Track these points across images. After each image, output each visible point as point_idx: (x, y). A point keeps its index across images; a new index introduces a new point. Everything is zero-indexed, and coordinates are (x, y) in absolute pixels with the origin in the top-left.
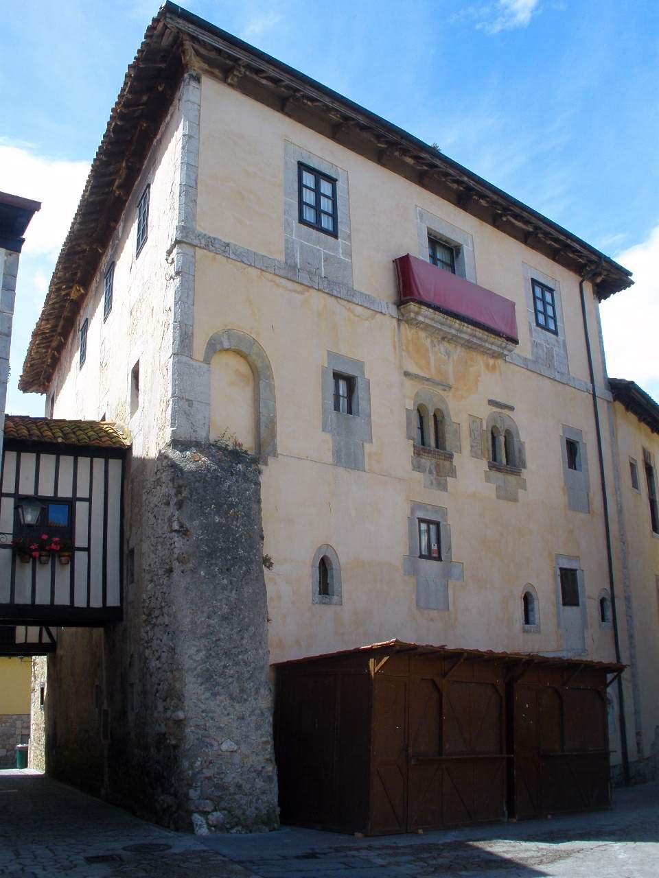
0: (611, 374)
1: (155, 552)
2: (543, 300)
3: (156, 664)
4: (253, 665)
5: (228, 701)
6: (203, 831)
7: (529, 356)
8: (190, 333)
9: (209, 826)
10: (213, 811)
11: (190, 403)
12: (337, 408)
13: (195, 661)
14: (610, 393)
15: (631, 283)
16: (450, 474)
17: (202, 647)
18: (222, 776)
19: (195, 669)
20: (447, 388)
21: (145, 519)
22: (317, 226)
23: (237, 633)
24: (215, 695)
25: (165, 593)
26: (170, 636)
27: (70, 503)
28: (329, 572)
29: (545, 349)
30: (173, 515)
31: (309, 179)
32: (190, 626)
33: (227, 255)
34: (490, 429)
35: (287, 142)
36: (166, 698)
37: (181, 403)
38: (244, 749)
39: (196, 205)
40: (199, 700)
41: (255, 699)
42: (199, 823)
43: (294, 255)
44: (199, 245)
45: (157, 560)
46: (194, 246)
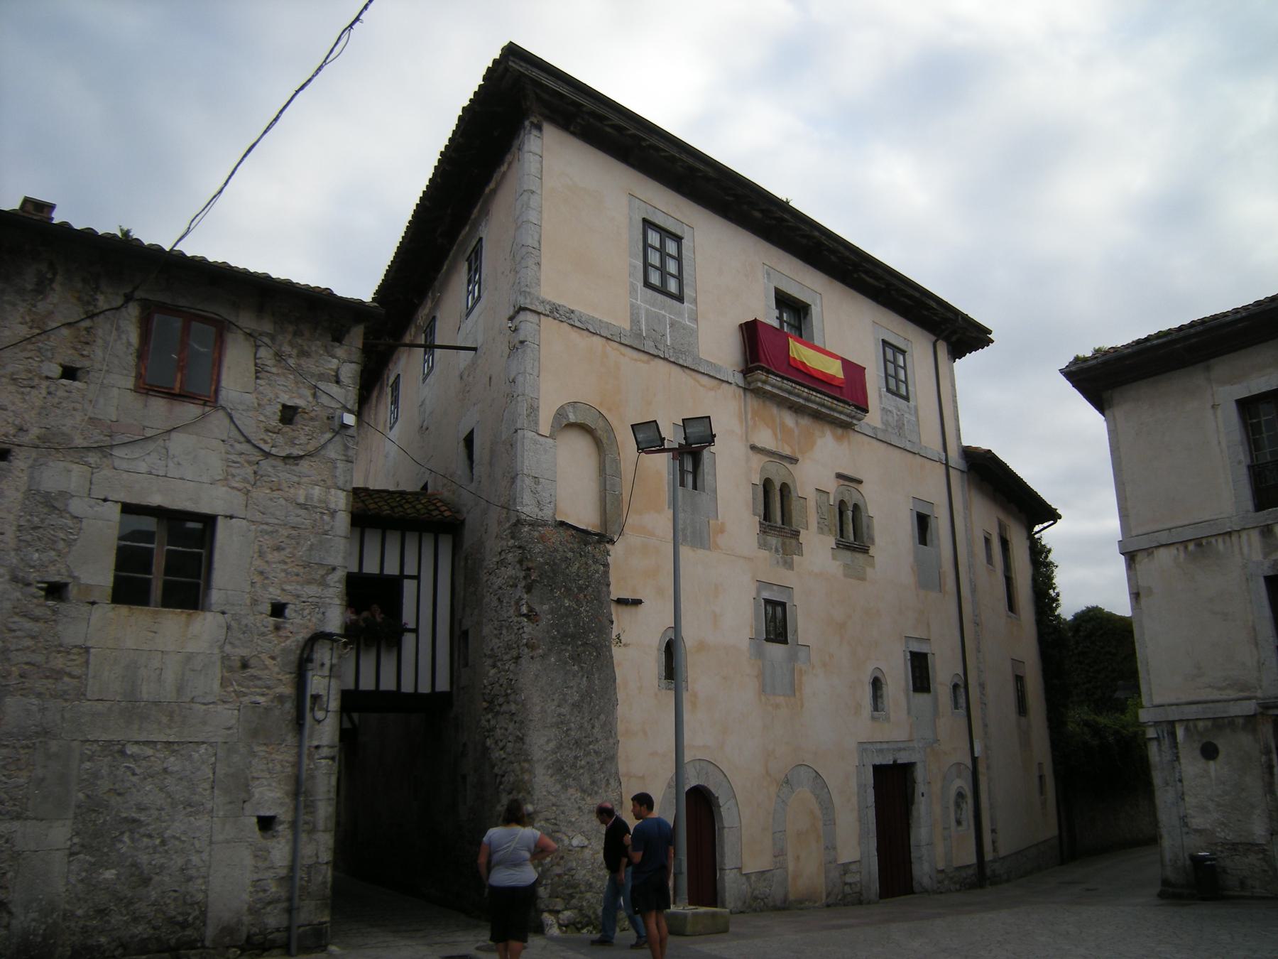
0: (966, 442)
1: (498, 636)
2: (895, 362)
3: (500, 755)
5: (579, 794)
6: (555, 931)
7: (879, 425)
9: (560, 926)
12: (682, 484)
13: (545, 751)
14: (964, 462)
19: (546, 759)
20: (793, 461)
21: (486, 600)
22: (663, 290)
24: (565, 787)
25: (511, 680)
26: (517, 724)
29: (895, 416)
30: (521, 599)
31: (654, 238)
33: (573, 323)
34: (837, 503)
36: (512, 790)
39: (540, 268)
40: (549, 793)
41: (606, 792)
42: (550, 922)
43: (639, 322)
44: (544, 312)
45: (501, 644)
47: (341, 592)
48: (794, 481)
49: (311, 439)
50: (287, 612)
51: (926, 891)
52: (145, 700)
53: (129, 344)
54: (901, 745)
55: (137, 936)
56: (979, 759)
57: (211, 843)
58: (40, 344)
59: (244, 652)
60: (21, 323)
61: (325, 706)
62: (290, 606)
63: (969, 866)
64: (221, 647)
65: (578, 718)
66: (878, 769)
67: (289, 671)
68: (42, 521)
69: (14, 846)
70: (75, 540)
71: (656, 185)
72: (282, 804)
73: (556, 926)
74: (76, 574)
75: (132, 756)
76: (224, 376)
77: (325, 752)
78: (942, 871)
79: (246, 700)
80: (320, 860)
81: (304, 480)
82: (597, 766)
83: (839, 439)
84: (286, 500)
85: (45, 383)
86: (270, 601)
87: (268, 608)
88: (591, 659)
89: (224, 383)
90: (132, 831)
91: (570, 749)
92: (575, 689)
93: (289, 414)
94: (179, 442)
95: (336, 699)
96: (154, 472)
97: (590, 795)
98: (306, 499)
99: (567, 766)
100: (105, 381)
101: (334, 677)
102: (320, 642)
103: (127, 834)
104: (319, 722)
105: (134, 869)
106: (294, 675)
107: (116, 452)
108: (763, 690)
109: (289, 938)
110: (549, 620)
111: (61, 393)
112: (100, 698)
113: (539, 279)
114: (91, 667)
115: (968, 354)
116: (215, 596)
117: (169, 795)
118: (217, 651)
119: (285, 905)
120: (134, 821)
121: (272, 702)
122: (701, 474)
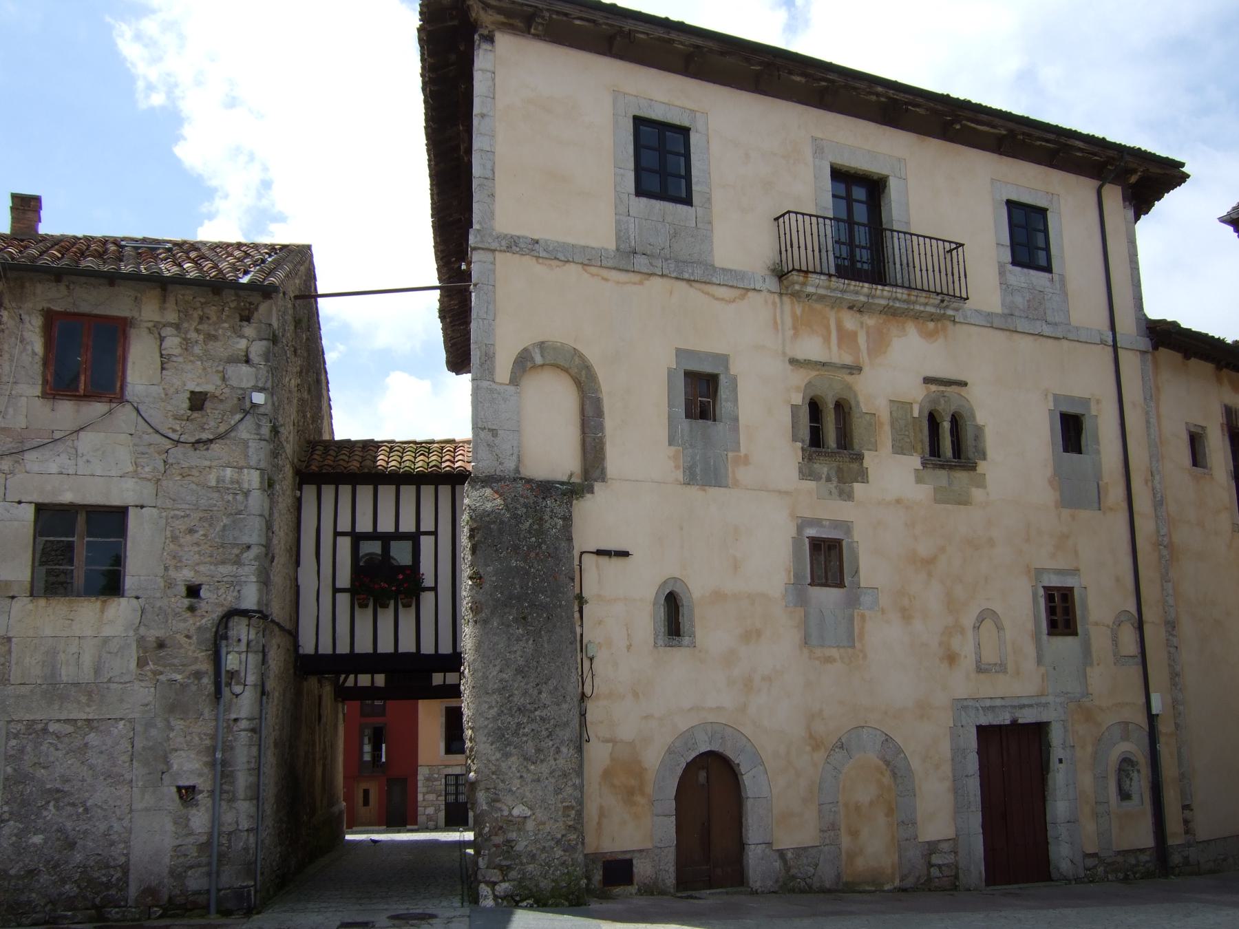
4: (552, 722)
6: (489, 903)
9: (496, 897)
10: (501, 882)
11: (494, 433)
15: (1184, 178)
19: (486, 726)
23: (533, 687)
24: (507, 756)
27: (414, 538)
28: (680, 608)
32: (481, 681)
33: (537, 255)
35: (616, 94)
37: (482, 434)
38: (540, 814)
41: (555, 760)
46: (493, 251)
47: (257, 569)
48: (856, 396)
49: (221, 423)
50: (202, 593)
51: (1067, 880)
52: (64, 682)
53: (34, 354)
54: (1026, 702)
55: (64, 894)
56: (1159, 719)
57: (131, 811)
59: (160, 633)
61: (243, 681)
62: (204, 588)
63: (1142, 851)
65: (522, 684)
66: (984, 732)
67: (204, 648)
71: (653, 72)
72: (200, 775)
73: (491, 897)
76: (129, 372)
77: (244, 724)
78: (1094, 855)
79: (162, 678)
80: (240, 827)
81: (214, 464)
82: (544, 733)
83: (929, 335)
84: (197, 485)
86: (183, 583)
87: (183, 590)
88: (539, 621)
89: (129, 379)
90: (57, 800)
92: (519, 653)
93: (198, 401)
94: (87, 441)
96: (65, 471)
98: (218, 482)
99: (508, 734)
100: (13, 392)
101: (251, 652)
102: (236, 618)
103: (52, 804)
104: (237, 696)
105: (59, 834)
107: (27, 456)
108: (806, 641)
109: (209, 900)
110: (494, 582)
112: (23, 682)
113: (492, 213)
114: (13, 655)
115: (1156, 202)
117: (91, 767)
118: (131, 633)
119: (204, 869)
120: (58, 791)
121: (188, 678)
122: (719, 401)
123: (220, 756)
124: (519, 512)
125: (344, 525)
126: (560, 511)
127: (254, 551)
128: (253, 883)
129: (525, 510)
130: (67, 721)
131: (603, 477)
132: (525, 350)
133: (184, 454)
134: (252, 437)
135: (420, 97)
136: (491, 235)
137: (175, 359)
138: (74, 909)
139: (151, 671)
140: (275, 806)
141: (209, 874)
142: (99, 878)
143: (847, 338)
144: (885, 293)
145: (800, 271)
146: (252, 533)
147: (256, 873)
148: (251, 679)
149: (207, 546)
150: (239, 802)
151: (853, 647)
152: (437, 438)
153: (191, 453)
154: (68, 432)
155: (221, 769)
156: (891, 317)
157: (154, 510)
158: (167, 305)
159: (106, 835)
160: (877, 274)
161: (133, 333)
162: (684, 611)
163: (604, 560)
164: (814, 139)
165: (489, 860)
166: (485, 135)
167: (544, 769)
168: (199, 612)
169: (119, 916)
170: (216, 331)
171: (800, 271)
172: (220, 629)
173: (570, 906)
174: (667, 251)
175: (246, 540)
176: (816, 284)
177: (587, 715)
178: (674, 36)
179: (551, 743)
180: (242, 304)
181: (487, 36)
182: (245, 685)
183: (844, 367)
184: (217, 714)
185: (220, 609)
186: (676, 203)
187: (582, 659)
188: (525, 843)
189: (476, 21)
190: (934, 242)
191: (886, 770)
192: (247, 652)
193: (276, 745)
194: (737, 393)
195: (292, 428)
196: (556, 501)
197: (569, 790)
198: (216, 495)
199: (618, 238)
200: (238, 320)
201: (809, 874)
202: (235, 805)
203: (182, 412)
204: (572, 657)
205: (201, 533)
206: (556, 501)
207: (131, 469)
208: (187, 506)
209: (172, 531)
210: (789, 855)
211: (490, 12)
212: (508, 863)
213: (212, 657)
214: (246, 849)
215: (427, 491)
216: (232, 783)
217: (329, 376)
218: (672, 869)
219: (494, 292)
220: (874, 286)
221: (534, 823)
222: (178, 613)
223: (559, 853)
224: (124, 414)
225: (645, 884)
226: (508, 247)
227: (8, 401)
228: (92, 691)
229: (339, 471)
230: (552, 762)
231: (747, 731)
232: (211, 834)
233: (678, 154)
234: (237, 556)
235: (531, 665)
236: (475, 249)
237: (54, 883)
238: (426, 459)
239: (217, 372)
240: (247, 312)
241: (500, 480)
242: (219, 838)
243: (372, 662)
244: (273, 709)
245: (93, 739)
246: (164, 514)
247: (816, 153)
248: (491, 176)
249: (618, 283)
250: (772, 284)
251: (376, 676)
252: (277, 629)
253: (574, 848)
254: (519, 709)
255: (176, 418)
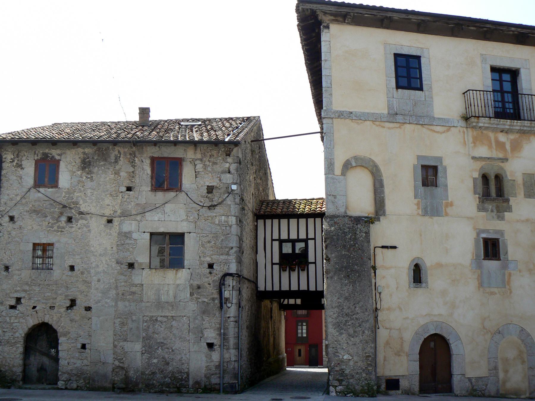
4: (361, 320)
6: (334, 394)
8: (333, 163)
9: (336, 392)
11: (335, 197)
16: (508, 210)
17: (335, 312)
18: (344, 370)
19: (332, 322)
23: (352, 305)
24: (341, 334)
27: (306, 241)
28: (421, 271)
35: (385, 44)
37: (330, 198)
38: (355, 358)
41: (362, 336)
48: (505, 172)
53: (148, 174)
57: (189, 352)
58: (118, 181)
59: (198, 283)
60: (112, 174)
61: (231, 302)
64: (189, 282)
68: (124, 242)
69: (125, 350)
70: (135, 247)
72: (215, 339)
73: (334, 392)
74: (137, 259)
75: (160, 321)
76: (183, 179)
77: (232, 319)
79: (200, 300)
80: (232, 360)
85: (121, 194)
87: (207, 266)
88: (355, 277)
89: (183, 182)
90: (162, 346)
91: (343, 317)
92: (346, 291)
93: (210, 189)
94: (168, 207)
95: (235, 299)
96: (160, 220)
97: (353, 337)
98: (219, 222)
102: (228, 277)
103: (160, 347)
104: (229, 308)
106: (218, 290)
108: (481, 285)
109: (220, 387)
111: (126, 197)
113: (331, 102)
116: (186, 263)
117: (174, 334)
118: (187, 283)
119: (218, 375)
120: (162, 343)
123: (223, 331)
124: (346, 231)
125: (276, 236)
126: (364, 230)
127: (234, 250)
128: (237, 382)
129: (348, 230)
130: (164, 316)
131: (384, 214)
132: (348, 160)
133: (206, 211)
134: (232, 203)
135: (302, 52)
136: (331, 111)
137: (201, 173)
138: (170, 388)
139: (195, 297)
140: (248, 352)
141: (220, 377)
142: (178, 377)
143: (501, 146)
144: (519, 124)
145: (475, 117)
146: (234, 242)
147: (238, 378)
148: (234, 301)
149: (215, 248)
150: (231, 350)
151: (505, 287)
152: (315, 198)
153: (208, 211)
154: (161, 205)
155: (224, 337)
156: (523, 135)
157: (194, 234)
158: (197, 152)
159: (180, 360)
160: (516, 115)
161: (184, 164)
162: (423, 272)
163: (385, 250)
164: (482, 55)
165: (334, 377)
166: (327, 69)
167: (357, 340)
168: (213, 275)
169: (186, 391)
170: (217, 160)
171: (475, 117)
172: (222, 281)
173: (369, 397)
174: (412, 112)
175: (231, 245)
176: (483, 122)
177: (378, 317)
178: (410, 17)
179: (360, 329)
180: (227, 149)
181: (326, 26)
182: (232, 303)
183: (500, 159)
184: (221, 315)
185: (222, 273)
186: (415, 90)
187: (376, 293)
188: (349, 370)
189: (321, 20)
190: (475, 92)
191: (522, 344)
192: (233, 290)
193: (247, 328)
194: (446, 174)
195: (251, 196)
196: (362, 225)
197: (369, 349)
198: (218, 227)
199: (389, 108)
200: (225, 156)
201: (483, 389)
202: (229, 351)
203: (204, 194)
204: (370, 292)
205: (213, 243)
206: (362, 225)
207: (185, 218)
208: (207, 232)
209: (202, 242)
210: (473, 380)
211: (327, 16)
212: (342, 378)
213: (219, 292)
214: (234, 368)
215: (311, 221)
216: (228, 342)
217: (271, 170)
218: (417, 384)
219: (333, 136)
220: (513, 121)
221: (353, 362)
222: (205, 275)
223: (364, 375)
224: (182, 196)
225: (405, 390)
226: (338, 116)
227: (139, 193)
228: (173, 305)
229: (272, 213)
230: (361, 337)
231: (453, 325)
232: (220, 362)
233: (416, 68)
234: (228, 252)
235: (351, 296)
236: (324, 118)
237: (162, 378)
238: (310, 207)
239: (218, 177)
240: (229, 152)
241: (338, 217)
242: (223, 364)
243: (290, 294)
244: (245, 315)
245: (174, 324)
246: (198, 236)
247: (483, 61)
248: (330, 86)
249: (389, 128)
250: (463, 123)
251: (297, 300)
252: (246, 281)
253: (371, 373)
254: (346, 314)
255: (202, 197)
